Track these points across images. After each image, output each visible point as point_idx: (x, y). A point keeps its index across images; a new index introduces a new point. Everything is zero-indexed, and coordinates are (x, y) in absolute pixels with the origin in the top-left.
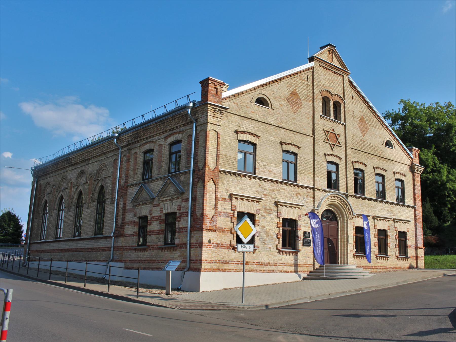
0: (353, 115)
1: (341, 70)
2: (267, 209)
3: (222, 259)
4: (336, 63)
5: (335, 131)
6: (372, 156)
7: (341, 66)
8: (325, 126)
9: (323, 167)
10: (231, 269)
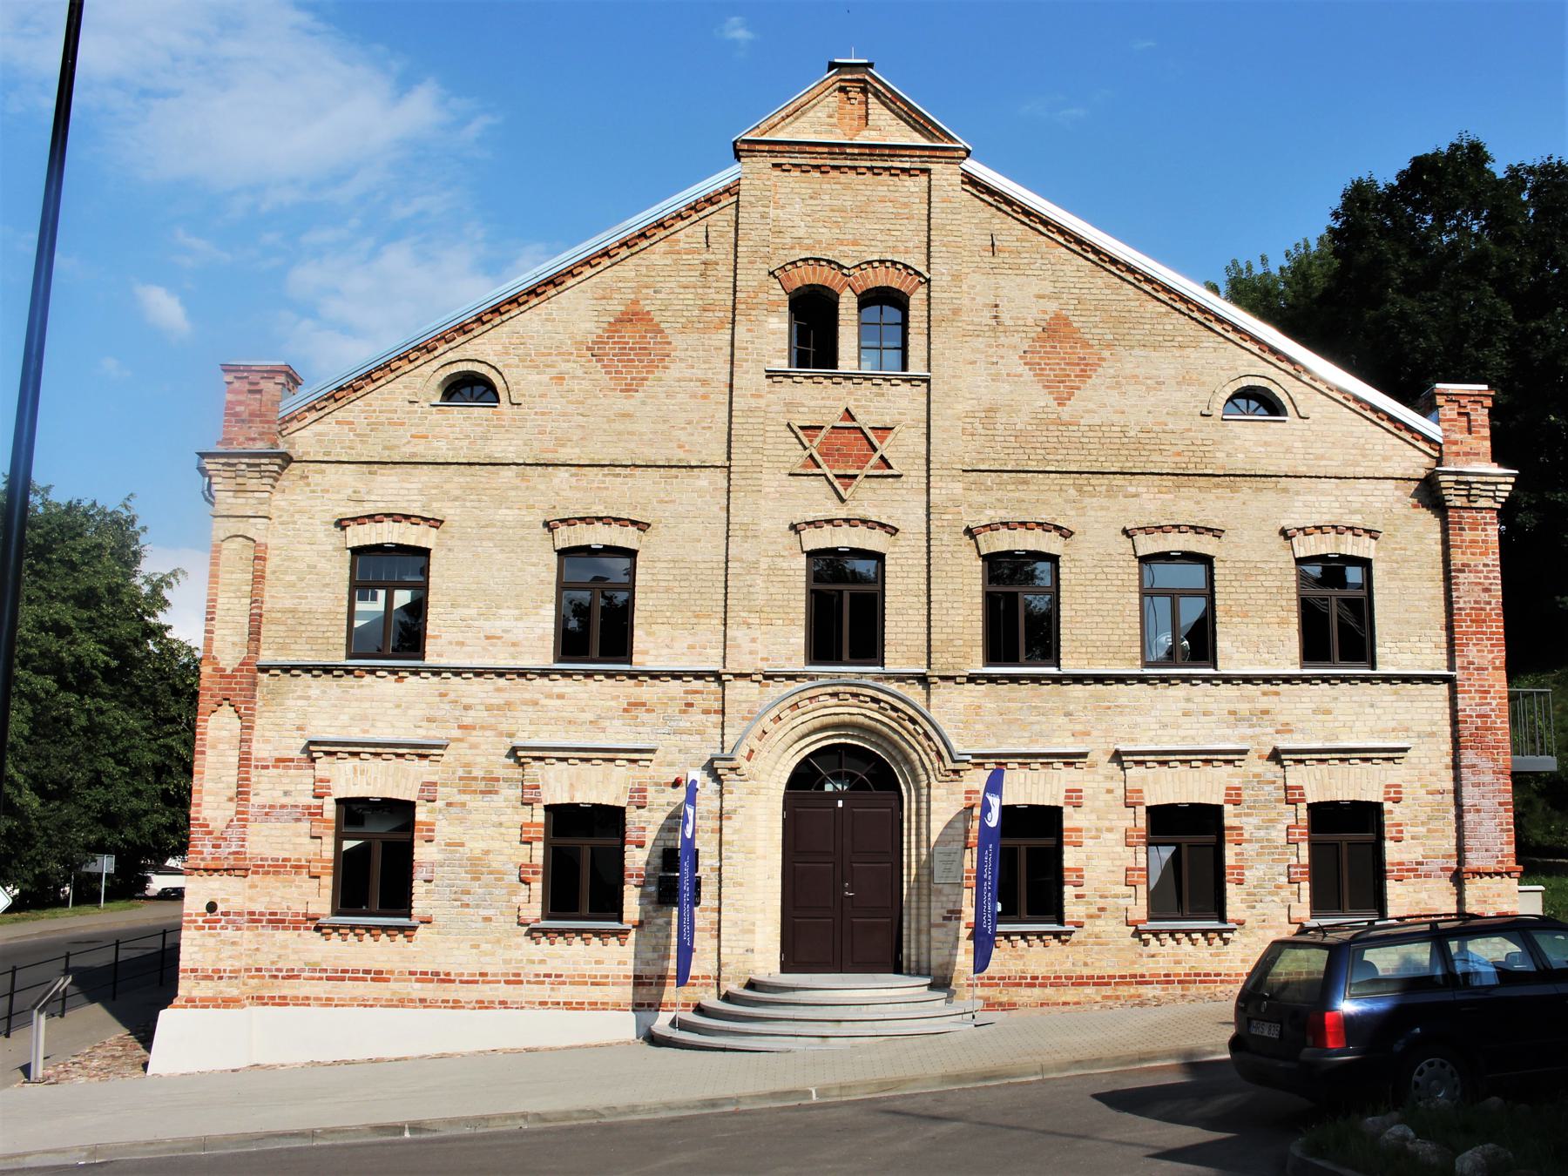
0: (993, 322)
1: (908, 153)
2: (475, 779)
3: (273, 963)
4: (888, 129)
5: (858, 417)
6: (1119, 480)
7: (917, 135)
8: (801, 409)
9: (785, 579)
10: (308, 998)
